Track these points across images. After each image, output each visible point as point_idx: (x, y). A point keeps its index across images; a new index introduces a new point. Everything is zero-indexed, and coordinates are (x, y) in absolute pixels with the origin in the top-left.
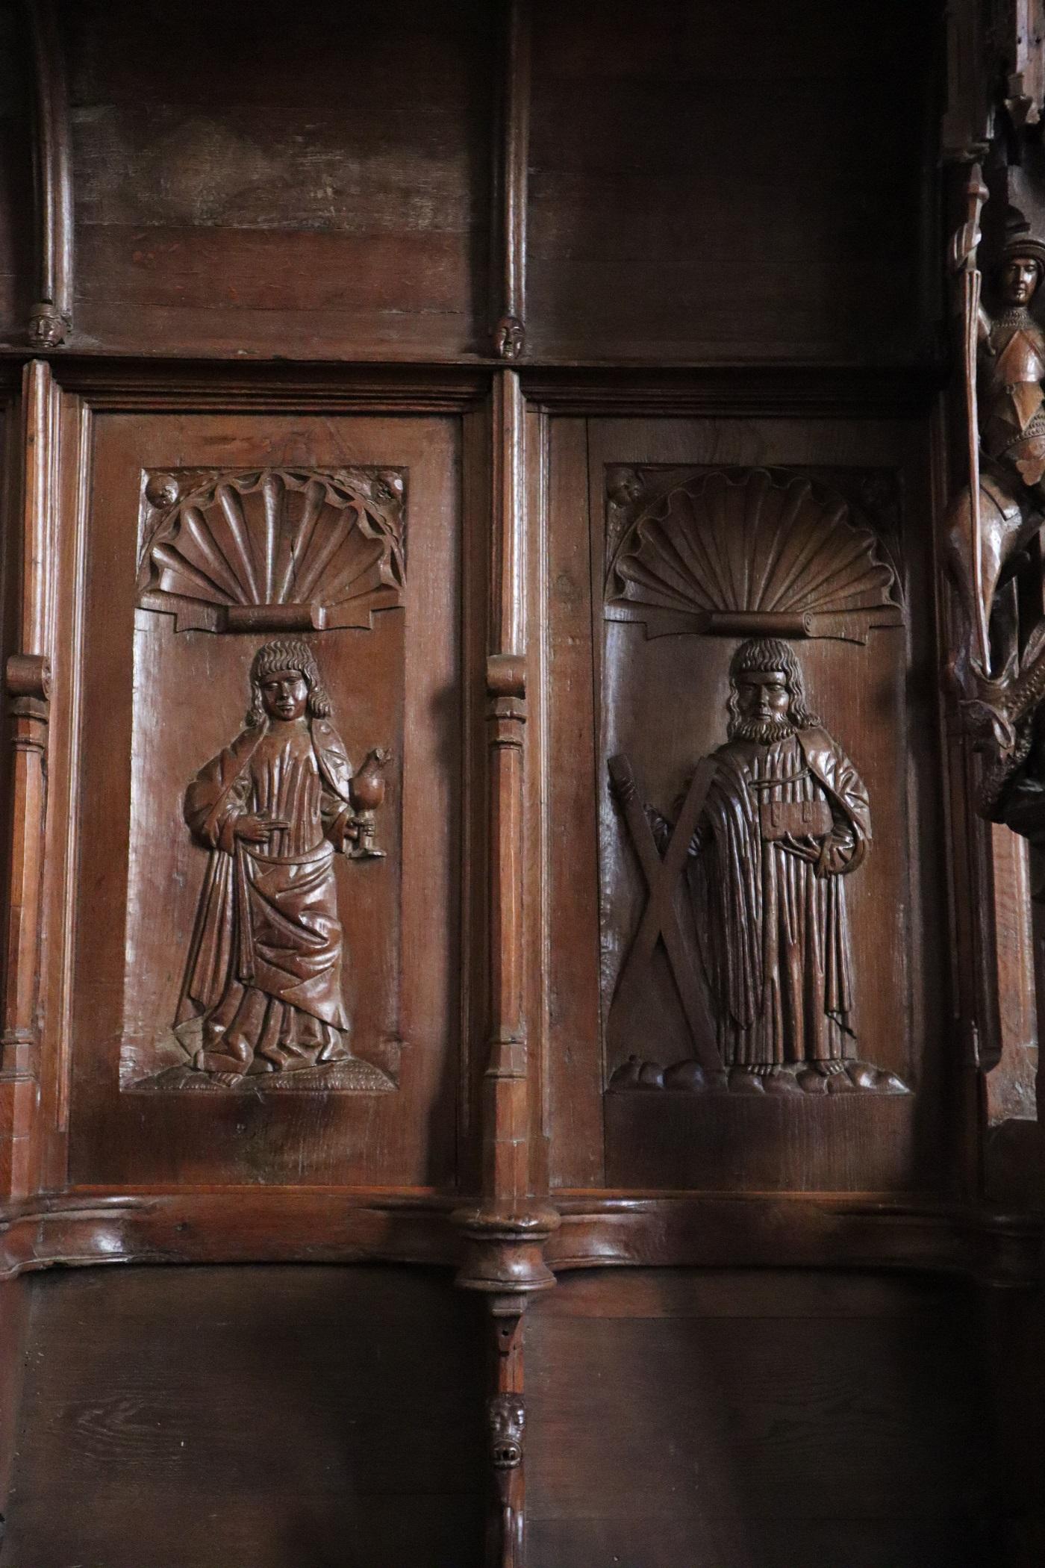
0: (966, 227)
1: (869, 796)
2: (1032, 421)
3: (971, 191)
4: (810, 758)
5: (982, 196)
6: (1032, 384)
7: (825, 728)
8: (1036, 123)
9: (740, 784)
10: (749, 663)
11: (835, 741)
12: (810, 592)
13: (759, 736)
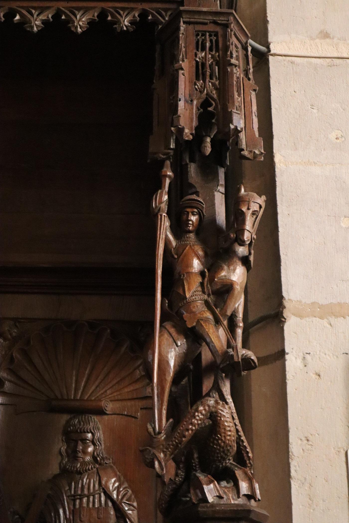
0: (159, 191)
1: (138, 505)
2: (193, 293)
3: (163, 173)
4: (103, 482)
5: (169, 177)
6: (196, 273)
7: (114, 465)
8: (184, 138)
9: (63, 497)
10: (72, 428)
11: (120, 472)
12: (108, 389)
13: (75, 469)
